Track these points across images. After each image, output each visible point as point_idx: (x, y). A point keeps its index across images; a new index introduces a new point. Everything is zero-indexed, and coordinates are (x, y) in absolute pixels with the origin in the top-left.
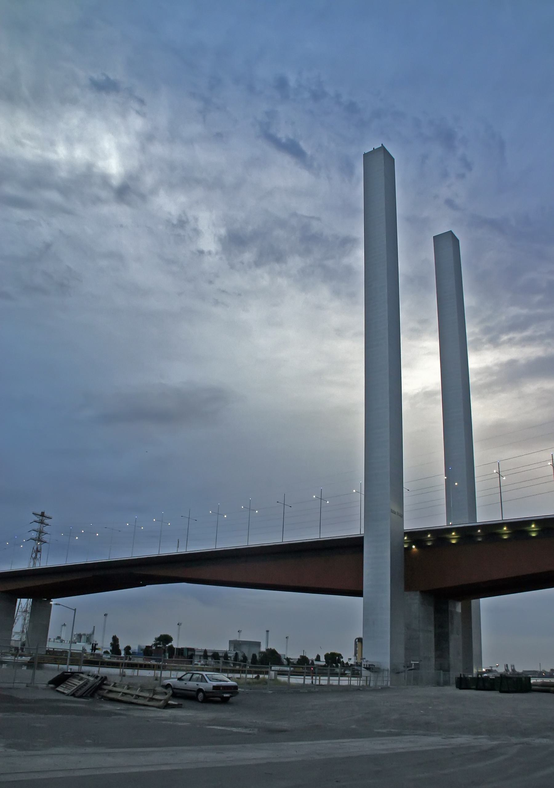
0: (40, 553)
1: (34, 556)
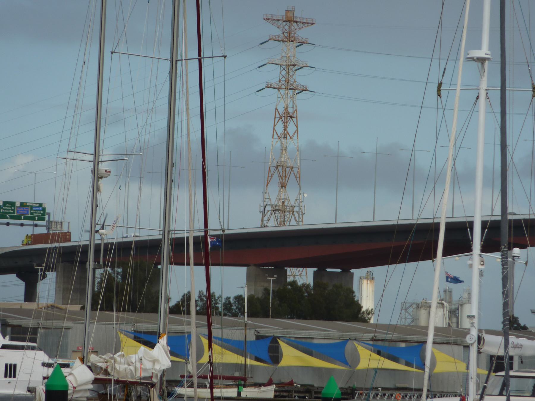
0: (294, 119)
1: (280, 128)
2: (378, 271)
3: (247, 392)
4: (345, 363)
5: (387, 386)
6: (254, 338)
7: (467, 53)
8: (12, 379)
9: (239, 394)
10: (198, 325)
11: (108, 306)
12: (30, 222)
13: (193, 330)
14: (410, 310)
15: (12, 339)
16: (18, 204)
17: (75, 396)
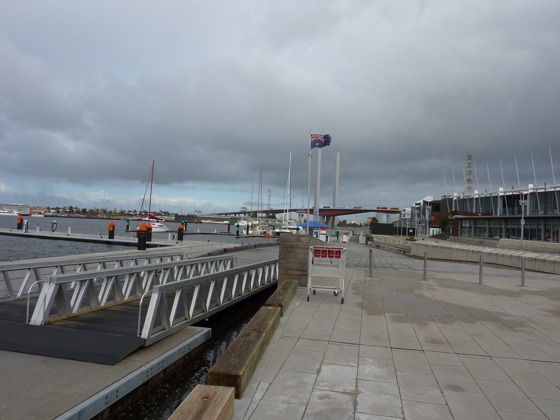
2: (278, 214)
3: (265, 225)
11: (253, 217)
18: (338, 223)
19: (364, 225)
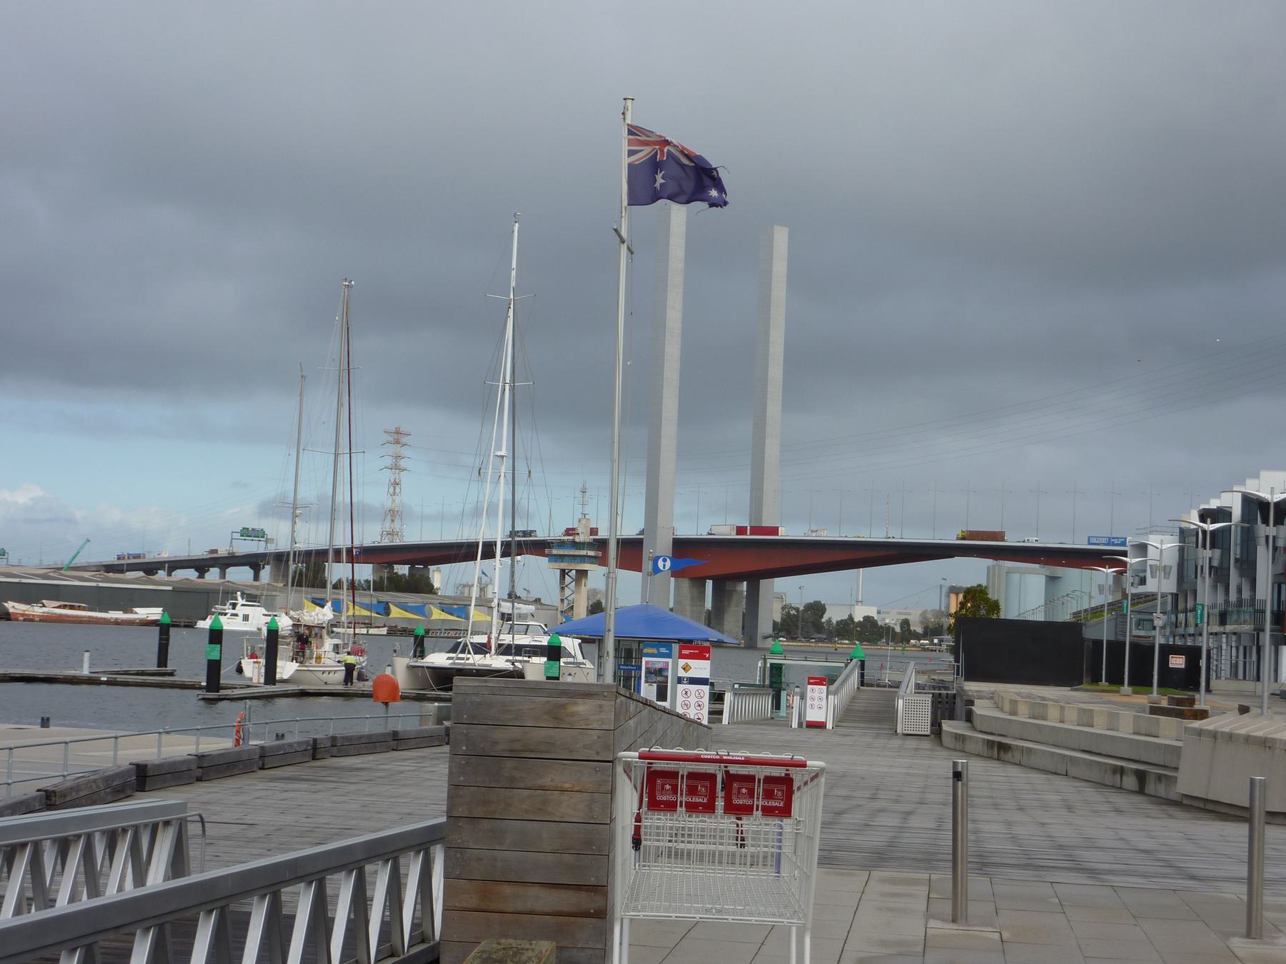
3: (372, 631)
4: (426, 617)
5: (447, 628)
6: (376, 602)
7: (494, 453)
8: (246, 622)
9: (368, 631)
10: (347, 595)
11: (300, 585)
12: (256, 539)
13: (345, 598)
14: (459, 588)
15: (247, 601)
16: (250, 529)
17: (283, 633)
18: (778, 620)
19: (920, 630)
